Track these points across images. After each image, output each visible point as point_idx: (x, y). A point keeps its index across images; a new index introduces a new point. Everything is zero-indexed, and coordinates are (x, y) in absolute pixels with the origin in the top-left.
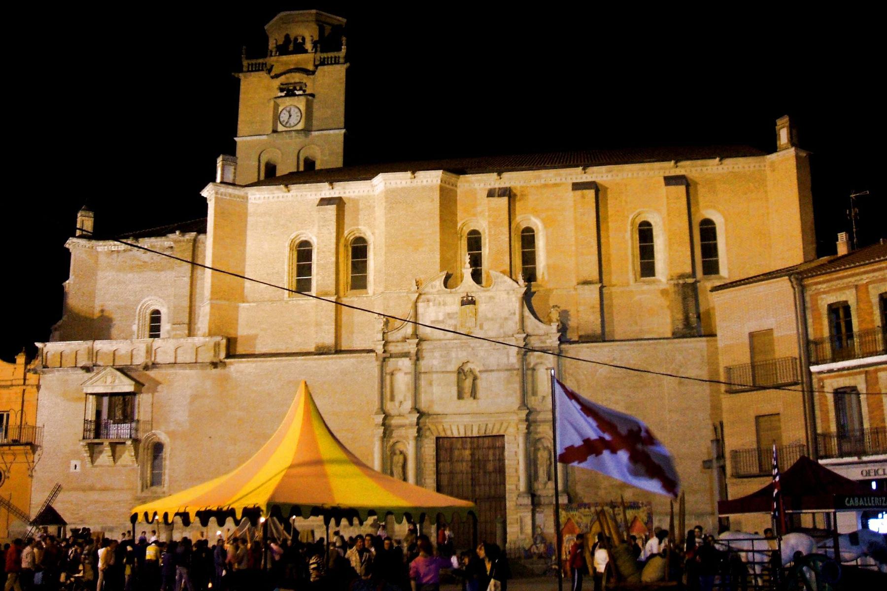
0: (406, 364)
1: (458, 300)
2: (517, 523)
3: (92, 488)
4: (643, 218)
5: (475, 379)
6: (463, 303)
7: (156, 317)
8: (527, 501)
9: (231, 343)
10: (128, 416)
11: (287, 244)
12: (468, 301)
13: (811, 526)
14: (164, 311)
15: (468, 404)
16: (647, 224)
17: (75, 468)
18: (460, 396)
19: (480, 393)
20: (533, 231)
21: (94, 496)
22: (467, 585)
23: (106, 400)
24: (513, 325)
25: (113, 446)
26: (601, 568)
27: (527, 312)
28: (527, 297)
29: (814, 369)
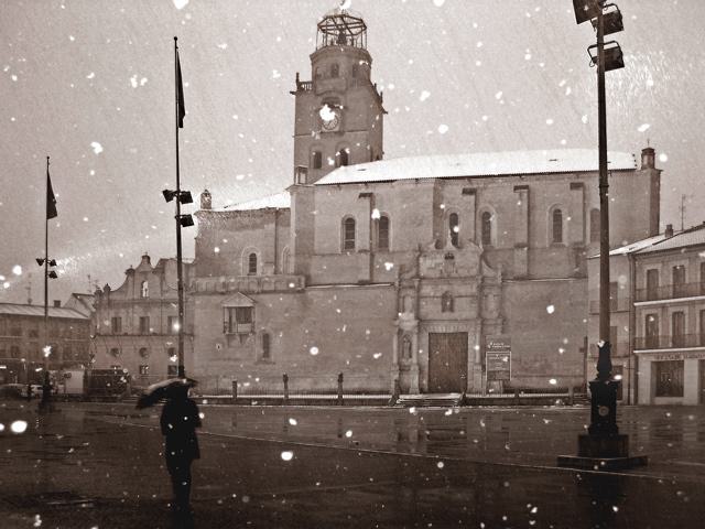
0: (411, 292)
1: (443, 256)
2: (506, 392)
3: (229, 359)
4: (560, 207)
5: (452, 302)
6: (446, 258)
7: (253, 258)
8: (480, 368)
9: (308, 278)
10: (248, 320)
11: (340, 222)
12: (450, 257)
13: (605, 41)
14: (258, 255)
15: (447, 315)
16: (559, 211)
17: (341, 376)
18: (443, 311)
19: (456, 308)
20: (368, 58)
21: (232, 363)
22: (680, 463)
23: (234, 311)
24: (474, 271)
25: (241, 336)
26: (380, 354)
27: (483, 263)
28: (483, 257)
29: (636, 304)
